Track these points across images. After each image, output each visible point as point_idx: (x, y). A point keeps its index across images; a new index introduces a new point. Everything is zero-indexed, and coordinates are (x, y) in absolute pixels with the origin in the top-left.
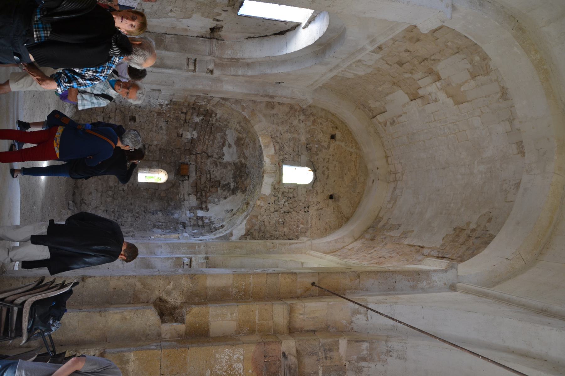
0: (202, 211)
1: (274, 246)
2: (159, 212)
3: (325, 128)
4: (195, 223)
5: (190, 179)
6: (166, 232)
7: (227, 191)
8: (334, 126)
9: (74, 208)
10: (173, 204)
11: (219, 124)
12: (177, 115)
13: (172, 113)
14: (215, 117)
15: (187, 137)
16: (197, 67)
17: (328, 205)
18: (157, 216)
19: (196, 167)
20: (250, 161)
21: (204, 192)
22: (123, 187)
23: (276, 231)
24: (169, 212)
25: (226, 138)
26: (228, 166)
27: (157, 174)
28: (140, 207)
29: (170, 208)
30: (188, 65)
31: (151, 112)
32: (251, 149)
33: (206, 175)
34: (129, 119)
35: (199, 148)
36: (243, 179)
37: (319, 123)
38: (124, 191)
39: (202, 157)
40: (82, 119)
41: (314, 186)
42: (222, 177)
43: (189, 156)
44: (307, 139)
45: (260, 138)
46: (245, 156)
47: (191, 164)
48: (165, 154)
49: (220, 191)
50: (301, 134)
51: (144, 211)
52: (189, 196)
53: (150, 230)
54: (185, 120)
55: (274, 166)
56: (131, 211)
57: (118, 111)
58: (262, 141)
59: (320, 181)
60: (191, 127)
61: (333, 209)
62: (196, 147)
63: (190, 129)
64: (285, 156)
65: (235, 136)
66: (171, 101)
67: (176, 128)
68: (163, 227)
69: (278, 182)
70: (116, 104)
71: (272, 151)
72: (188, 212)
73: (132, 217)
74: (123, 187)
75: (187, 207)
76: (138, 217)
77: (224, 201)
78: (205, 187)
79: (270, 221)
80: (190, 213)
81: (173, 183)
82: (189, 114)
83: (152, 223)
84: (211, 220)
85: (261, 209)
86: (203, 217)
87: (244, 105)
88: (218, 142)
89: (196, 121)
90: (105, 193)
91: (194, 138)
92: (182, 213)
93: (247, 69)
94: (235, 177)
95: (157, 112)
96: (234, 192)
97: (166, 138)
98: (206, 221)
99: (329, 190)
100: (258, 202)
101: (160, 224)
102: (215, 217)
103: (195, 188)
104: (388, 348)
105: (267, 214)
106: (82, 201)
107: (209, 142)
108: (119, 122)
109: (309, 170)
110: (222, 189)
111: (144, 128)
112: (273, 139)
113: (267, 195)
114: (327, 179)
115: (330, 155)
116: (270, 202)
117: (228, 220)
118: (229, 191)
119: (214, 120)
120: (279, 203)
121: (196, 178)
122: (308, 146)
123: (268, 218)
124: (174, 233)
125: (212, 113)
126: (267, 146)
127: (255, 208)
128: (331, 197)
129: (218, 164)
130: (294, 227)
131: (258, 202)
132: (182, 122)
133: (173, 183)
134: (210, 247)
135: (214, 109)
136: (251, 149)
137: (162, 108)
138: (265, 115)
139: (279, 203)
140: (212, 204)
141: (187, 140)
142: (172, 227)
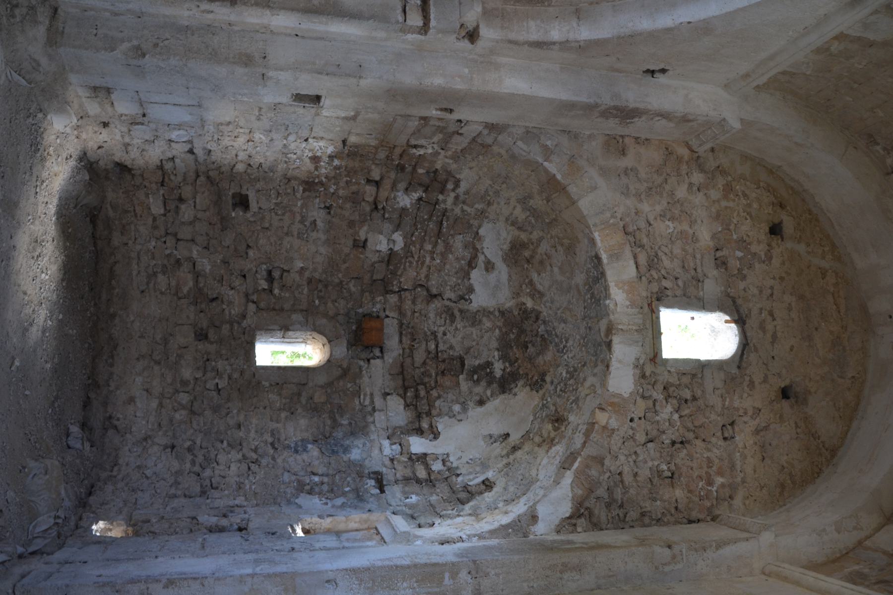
0: (423, 440)
1: (674, 557)
2: (310, 446)
3: (755, 205)
4: (408, 472)
5: (385, 355)
6: (333, 506)
7: (483, 383)
8: (775, 201)
9: (83, 444)
10: (345, 422)
11: (463, 211)
12: (354, 188)
13: (342, 184)
14: (453, 190)
15: (378, 248)
16: (432, 16)
17: (781, 417)
18: (305, 456)
19: (401, 325)
20: (552, 303)
21: (423, 387)
22: (217, 381)
23: (655, 500)
24: (336, 445)
25: (478, 247)
26: (485, 320)
27: (303, 345)
28: (262, 434)
29: (339, 434)
30: (404, 11)
31: (289, 180)
32: (556, 270)
33: (427, 345)
34: (230, 202)
35: (408, 276)
36: (531, 350)
37: (740, 194)
38: (219, 390)
39: (415, 298)
40: (108, 206)
41: (744, 365)
42: (469, 348)
43: (382, 298)
44: (714, 237)
46: (536, 290)
47: (387, 317)
48: (322, 294)
49: (464, 385)
50: (699, 222)
51: (272, 444)
52: (385, 399)
53: (289, 502)
54: (375, 203)
55: (639, 313)
56: (237, 445)
57: (202, 179)
58: (602, 241)
59: (756, 350)
61: (794, 425)
62: (399, 273)
63: (387, 227)
64: (665, 283)
65: (505, 239)
66: (344, 142)
67: (351, 224)
68: (325, 488)
69: (652, 356)
70: (196, 160)
71: (631, 271)
72: (386, 443)
73: (240, 461)
74: (217, 381)
75: (383, 429)
76: (257, 459)
77: (480, 410)
78: (426, 374)
79: (636, 470)
80: (391, 444)
81: (345, 366)
82: (387, 184)
83: (293, 478)
84: (448, 464)
85: (609, 436)
86: (425, 455)
87: (549, 143)
88: (457, 259)
89: (402, 204)
90: (170, 398)
91: (396, 249)
93: (575, 25)
94: (504, 347)
95: (304, 181)
96: (505, 385)
97: (324, 253)
98: (437, 466)
99: (779, 375)
100: (602, 418)
101: (316, 479)
102: (460, 454)
103: (401, 377)
105: (626, 452)
106: (107, 423)
107: (433, 259)
108: (205, 211)
109: (726, 322)
110: (470, 377)
111: (271, 225)
112: (629, 237)
113: (626, 395)
114: (773, 343)
115: (774, 278)
116: (633, 415)
117: (500, 465)
118: (489, 383)
119: (450, 200)
120: (658, 418)
121: (401, 352)
122: (719, 254)
123: (632, 463)
124: (356, 507)
125: (446, 181)
126: (615, 256)
127: (594, 435)
128: (785, 393)
129: (457, 313)
130: (701, 484)
131: (602, 418)
132: (368, 209)
133: (345, 366)
134: (487, 575)
135: (453, 166)
136: (556, 270)
137: (316, 168)
138: (604, 172)
139: (658, 418)
140: (446, 418)
141: (377, 254)
142: (347, 489)
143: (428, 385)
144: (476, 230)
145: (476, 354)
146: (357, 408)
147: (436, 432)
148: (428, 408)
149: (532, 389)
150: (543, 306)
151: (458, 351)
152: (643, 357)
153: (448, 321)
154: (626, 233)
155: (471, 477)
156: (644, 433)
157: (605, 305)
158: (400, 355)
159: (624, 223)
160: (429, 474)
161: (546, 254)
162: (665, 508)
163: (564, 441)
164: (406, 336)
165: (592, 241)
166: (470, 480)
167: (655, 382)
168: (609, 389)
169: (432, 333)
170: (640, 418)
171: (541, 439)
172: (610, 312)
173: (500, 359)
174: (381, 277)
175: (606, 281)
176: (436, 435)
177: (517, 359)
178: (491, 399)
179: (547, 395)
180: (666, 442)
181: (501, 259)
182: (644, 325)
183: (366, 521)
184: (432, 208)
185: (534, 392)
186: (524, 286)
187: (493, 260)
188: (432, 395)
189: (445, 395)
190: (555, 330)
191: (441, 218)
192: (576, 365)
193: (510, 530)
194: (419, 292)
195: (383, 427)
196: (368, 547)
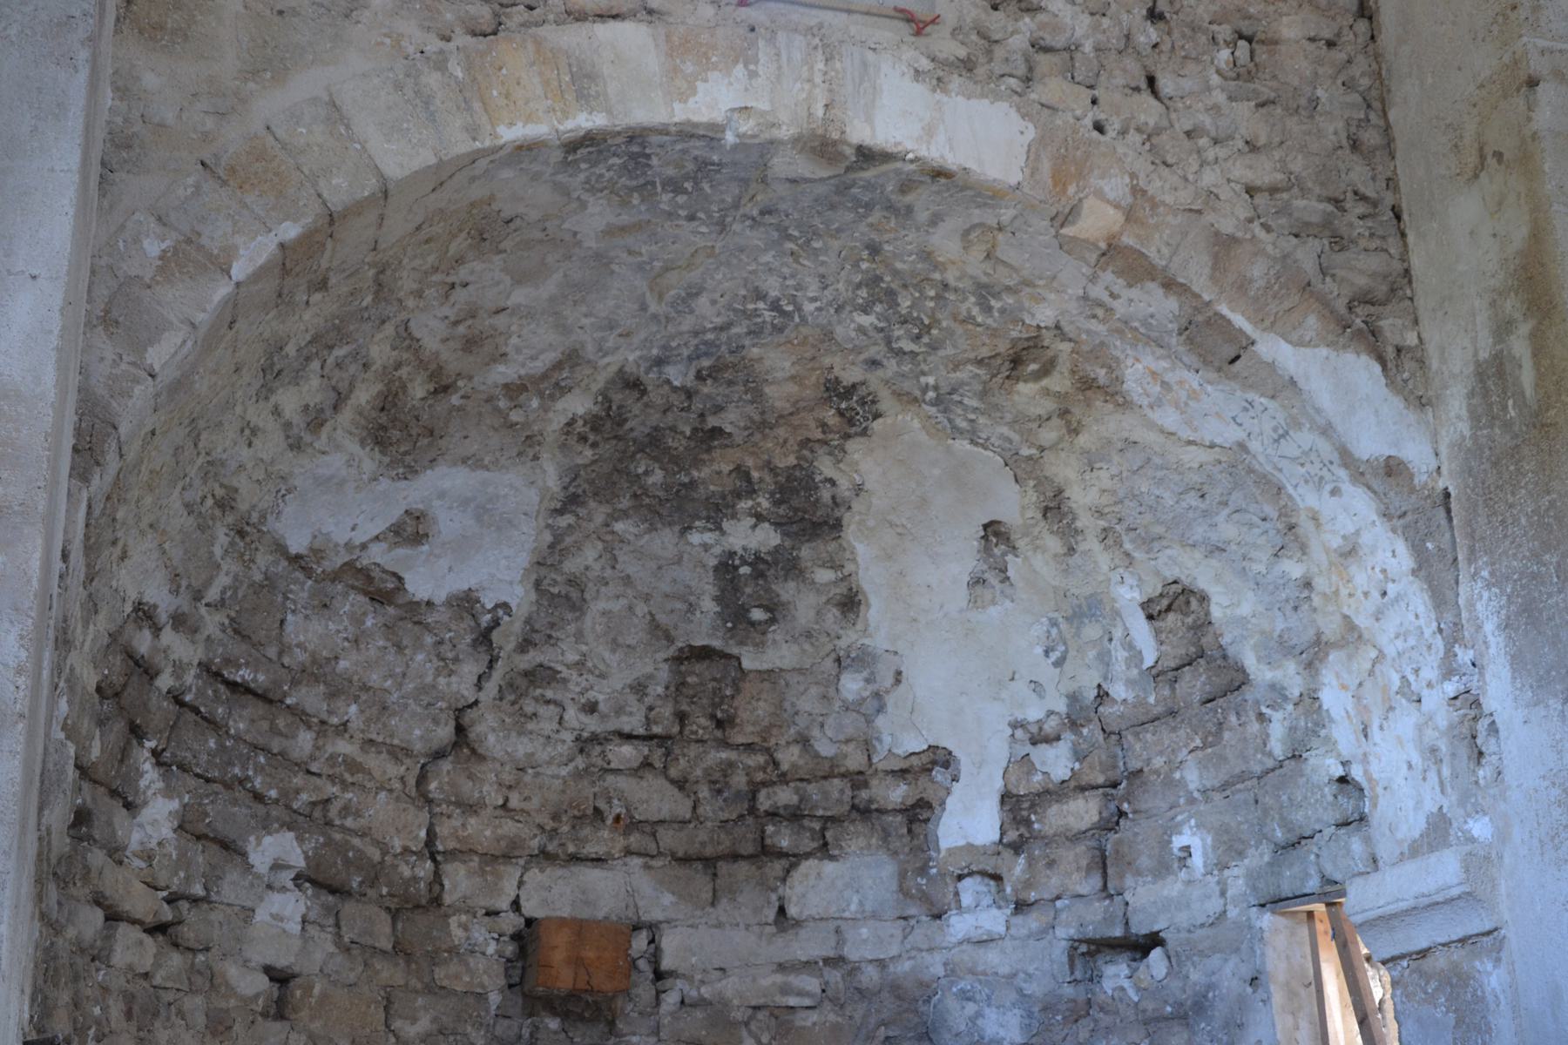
4: (1074, 857)
5: (645, 918)
7: (787, 590)
11: (219, 605)
15: (295, 927)
19: (545, 857)
23: (1314, 103)
25: (338, 560)
26: (572, 566)
32: (519, 297)
33: (617, 771)
36: (730, 420)
39: (458, 804)
42: (654, 627)
43: (453, 921)
45: (510, 133)
46: (545, 376)
49: (778, 653)
52: (798, 923)
54: (158, 929)
55: (772, 40)
58: (529, 119)
60: (212, 878)
63: (231, 889)
69: (905, 29)
72: (959, 925)
77: (875, 611)
79: (1240, 144)
84: (1051, 726)
85: (1154, 205)
86: (1006, 797)
87: (153, 247)
89: (167, 831)
92: (972, 972)
98: (1057, 762)
102: (1021, 687)
103: (723, 868)
104: (525, 351)
113: (1031, 133)
116: (1088, 122)
117: (1104, 560)
120: (1088, 47)
121: (637, 861)
123: (1221, 152)
136: (519, 297)
139: (1088, 47)
140: (880, 721)
141: (313, 931)
143: (760, 776)
144: (284, 563)
145: (679, 605)
146: (832, 1017)
147: (925, 759)
148: (836, 781)
149: (864, 433)
150: (606, 360)
151: (655, 667)
152: (908, 54)
153: (549, 694)
154: (495, 33)
155: (1120, 655)
156: (1136, 96)
157: (735, 148)
158: (647, 867)
159: (458, 30)
160: (1082, 789)
161: (456, 323)
162: (1334, 78)
163: (1118, 347)
164: (584, 841)
165: (526, 150)
166: (1136, 656)
167: (982, 35)
168: (1013, 181)
169: (581, 751)
170: (1094, 102)
171: (1056, 421)
172: (766, 136)
173: (719, 528)
174: (385, 918)
175: (663, 130)
176: (939, 759)
177: (738, 468)
178: (849, 568)
179: (907, 385)
180: (1154, 37)
181: (403, 484)
182: (809, 31)
183: (1292, 994)
184: (190, 716)
185: (877, 425)
186: (515, 416)
187: (396, 513)
188: (794, 766)
189: (802, 721)
190: (704, 331)
191: (222, 688)
192: (858, 278)
193: (1429, 545)
194: (440, 788)
195: (898, 933)
196: (939, 1000)
